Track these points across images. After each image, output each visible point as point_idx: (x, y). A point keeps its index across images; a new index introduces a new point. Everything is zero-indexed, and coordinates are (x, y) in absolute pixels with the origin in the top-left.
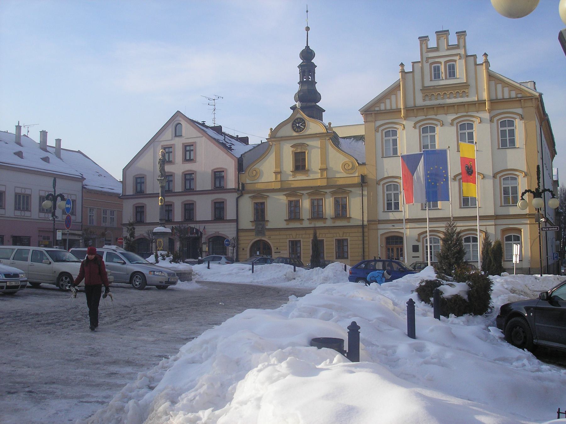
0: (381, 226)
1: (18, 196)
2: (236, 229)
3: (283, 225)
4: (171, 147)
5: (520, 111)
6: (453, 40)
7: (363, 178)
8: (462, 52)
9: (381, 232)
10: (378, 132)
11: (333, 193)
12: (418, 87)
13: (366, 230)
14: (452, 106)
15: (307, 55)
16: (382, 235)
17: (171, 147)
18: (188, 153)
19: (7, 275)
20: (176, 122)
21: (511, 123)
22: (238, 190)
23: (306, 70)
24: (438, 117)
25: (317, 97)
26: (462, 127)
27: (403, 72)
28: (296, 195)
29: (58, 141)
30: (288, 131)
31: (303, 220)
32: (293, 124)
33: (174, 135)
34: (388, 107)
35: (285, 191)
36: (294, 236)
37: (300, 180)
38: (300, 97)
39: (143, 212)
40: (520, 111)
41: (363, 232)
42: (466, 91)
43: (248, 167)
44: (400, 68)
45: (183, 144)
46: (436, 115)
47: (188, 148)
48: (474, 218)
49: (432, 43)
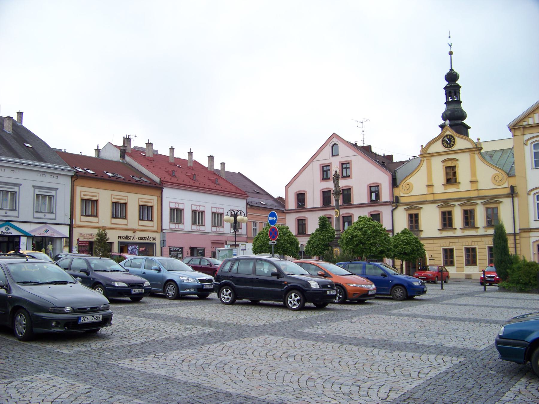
0: (532, 234)
1: (194, 212)
3: (438, 234)
4: (329, 166)
7: (512, 188)
9: (533, 240)
10: (526, 145)
13: (517, 237)
16: (534, 242)
18: (344, 170)
19: (201, 280)
20: (334, 143)
23: (452, 91)
25: (463, 116)
28: (472, 204)
29: (223, 164)
30: (439, 147)
31: (455, 229)
32: (443, 141)
33: (331, 155)
36: (447, 245)
37: (452, 191)
39: (305, 224)
41: (515, 240)
43: (401, 183)
45: (340, 162)
47: (344, 166)
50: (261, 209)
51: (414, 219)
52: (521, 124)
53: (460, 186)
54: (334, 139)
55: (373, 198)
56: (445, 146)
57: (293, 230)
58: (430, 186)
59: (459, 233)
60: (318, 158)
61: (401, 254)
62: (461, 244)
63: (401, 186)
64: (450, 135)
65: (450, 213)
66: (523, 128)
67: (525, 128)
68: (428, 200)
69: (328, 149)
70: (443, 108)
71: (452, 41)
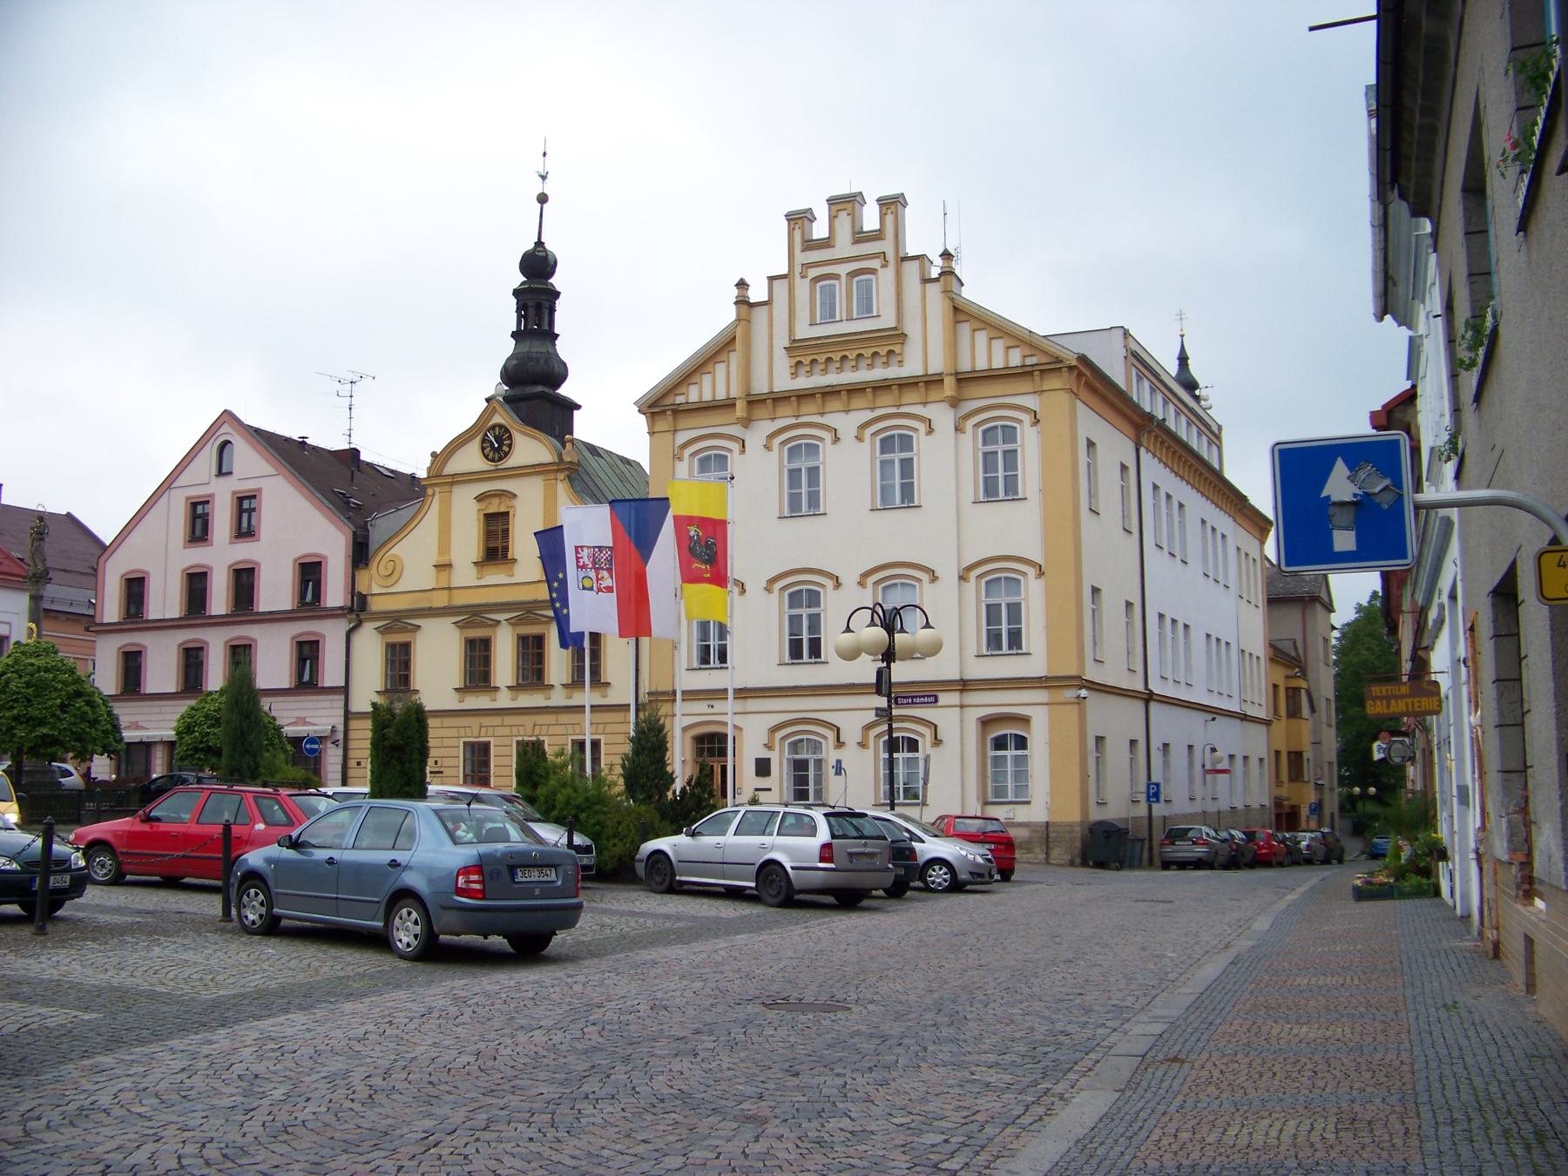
2: (342, 712)
3: (453, 703)
4: (254, 497)
5: (1030, 402)
6: (870, 219)
8: (887, 246)
10: (680, 459)
11: (514, 623)
12: (782, 341)
14: (854, 390)
15: (538, 265)
16: (685, 729)
17: (254, 497)
21: (1010, 434)
22: (351, 610)
23: (531, 303)
24: (827, 420)
25: (558, 374)
26: (887, 445)
27: (742, 302)
28: (403, 630)
30: (472, 459)
31: (497, 689)
32: (483, 441)
33: (214, 470)
34: (707, 397)
35: (378, 619)
37: (499, 584)
38: (513, 374)
40: (1030, 402)
42: (897, 349)
44: (735, 292)
45: (234, 493)
46: (822, 414)
48: (721, 694)
49: (820, 230)
50: (63, 617)
51: (399, 661)
52: (669, 401)
53: (517, 568)
54: (226, 428)
55: (309, 598)
56: (486, 457)
57: (106, 679)
58: (444, 567)
59: (504, 700)
60: (183, 479)
61: (197, 750)
62: (507, 731)
63: (374, 565)
64: (501, 426)
65: (486, 644)
66: (675, 412)
67: (678, 412)
68: (435, 605)
69: (209, 454)
70: (507, 347)
71: (551, 166)
